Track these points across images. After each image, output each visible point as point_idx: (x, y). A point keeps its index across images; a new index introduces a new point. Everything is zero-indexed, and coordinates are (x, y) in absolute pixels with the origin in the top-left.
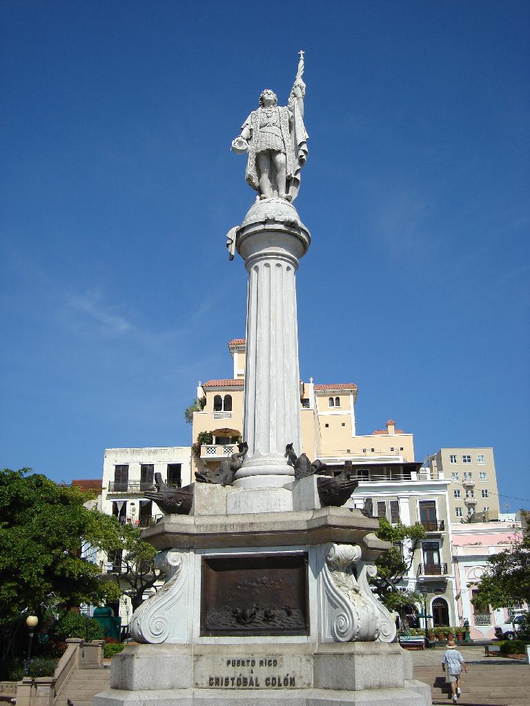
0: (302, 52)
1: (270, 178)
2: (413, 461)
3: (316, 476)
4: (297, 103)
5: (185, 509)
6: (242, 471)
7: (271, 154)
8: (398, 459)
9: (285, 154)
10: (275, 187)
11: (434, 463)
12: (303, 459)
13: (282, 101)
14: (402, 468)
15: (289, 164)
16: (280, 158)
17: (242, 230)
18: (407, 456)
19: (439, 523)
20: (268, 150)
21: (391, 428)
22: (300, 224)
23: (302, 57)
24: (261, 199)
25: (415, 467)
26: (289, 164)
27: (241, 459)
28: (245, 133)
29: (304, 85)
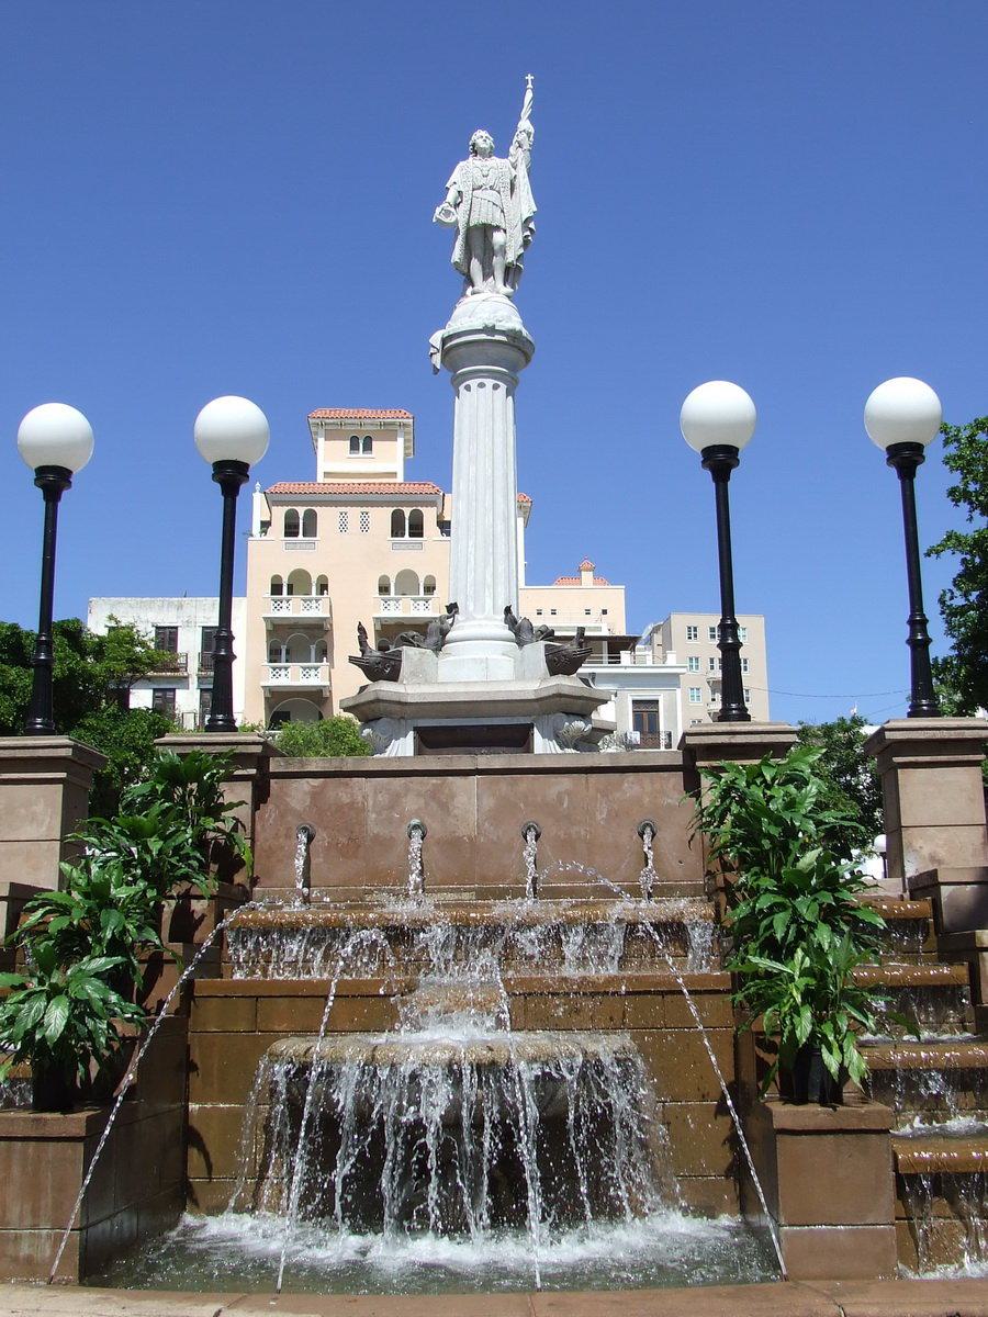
0: (529, 78)
1: (482, 263)
2: (623, 634)
3: (543, 643)
4: (520, 154)
5: (394, 676)
6: (449, 636)
7: (487, 230)
8: (599, 629)
9: (505, 231)
10: (488, 273)
11: (658, 638)
12: (526, 623)
13: (501, 150)
14: (605, 644)
15: (510, 242)
16: (498, 238)
17: (451, 337)
18: (615, 625)
19: (663, 736)
20: (484, 224)
21: (587, 577)
22: (525, 332)
23: (530, 86)
24: (473, 293)
25: (628, 643)
26: (510, 242)
27: (450, 621)
28: (451, 196)
29: (532, 130)
